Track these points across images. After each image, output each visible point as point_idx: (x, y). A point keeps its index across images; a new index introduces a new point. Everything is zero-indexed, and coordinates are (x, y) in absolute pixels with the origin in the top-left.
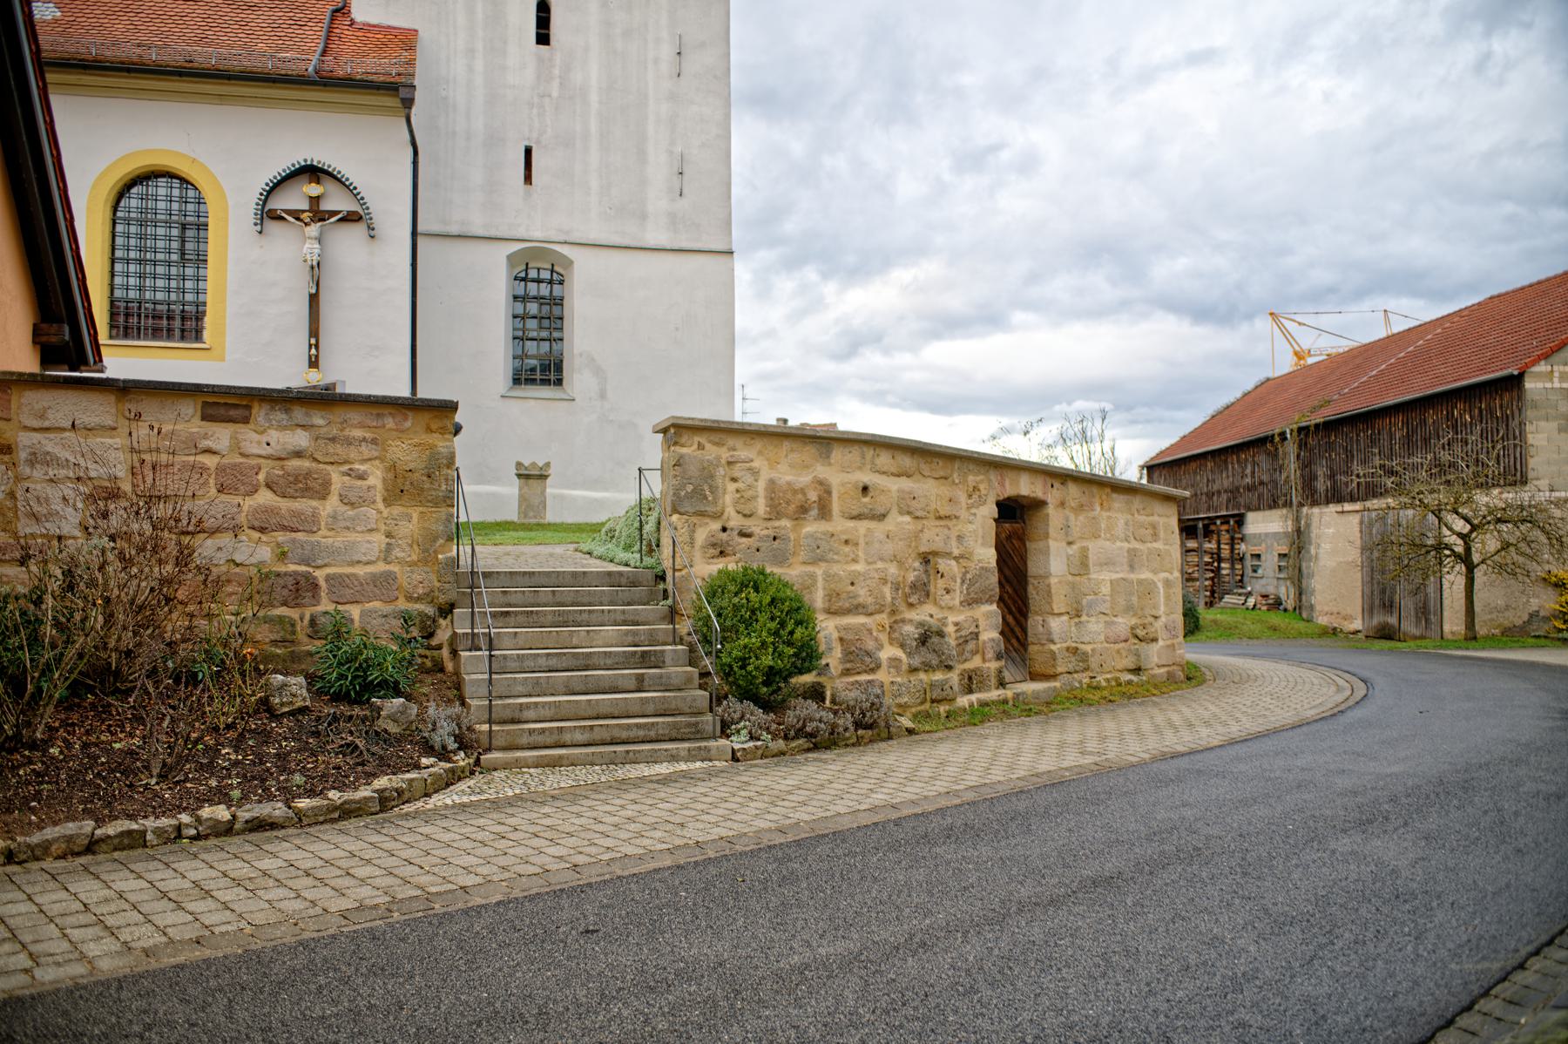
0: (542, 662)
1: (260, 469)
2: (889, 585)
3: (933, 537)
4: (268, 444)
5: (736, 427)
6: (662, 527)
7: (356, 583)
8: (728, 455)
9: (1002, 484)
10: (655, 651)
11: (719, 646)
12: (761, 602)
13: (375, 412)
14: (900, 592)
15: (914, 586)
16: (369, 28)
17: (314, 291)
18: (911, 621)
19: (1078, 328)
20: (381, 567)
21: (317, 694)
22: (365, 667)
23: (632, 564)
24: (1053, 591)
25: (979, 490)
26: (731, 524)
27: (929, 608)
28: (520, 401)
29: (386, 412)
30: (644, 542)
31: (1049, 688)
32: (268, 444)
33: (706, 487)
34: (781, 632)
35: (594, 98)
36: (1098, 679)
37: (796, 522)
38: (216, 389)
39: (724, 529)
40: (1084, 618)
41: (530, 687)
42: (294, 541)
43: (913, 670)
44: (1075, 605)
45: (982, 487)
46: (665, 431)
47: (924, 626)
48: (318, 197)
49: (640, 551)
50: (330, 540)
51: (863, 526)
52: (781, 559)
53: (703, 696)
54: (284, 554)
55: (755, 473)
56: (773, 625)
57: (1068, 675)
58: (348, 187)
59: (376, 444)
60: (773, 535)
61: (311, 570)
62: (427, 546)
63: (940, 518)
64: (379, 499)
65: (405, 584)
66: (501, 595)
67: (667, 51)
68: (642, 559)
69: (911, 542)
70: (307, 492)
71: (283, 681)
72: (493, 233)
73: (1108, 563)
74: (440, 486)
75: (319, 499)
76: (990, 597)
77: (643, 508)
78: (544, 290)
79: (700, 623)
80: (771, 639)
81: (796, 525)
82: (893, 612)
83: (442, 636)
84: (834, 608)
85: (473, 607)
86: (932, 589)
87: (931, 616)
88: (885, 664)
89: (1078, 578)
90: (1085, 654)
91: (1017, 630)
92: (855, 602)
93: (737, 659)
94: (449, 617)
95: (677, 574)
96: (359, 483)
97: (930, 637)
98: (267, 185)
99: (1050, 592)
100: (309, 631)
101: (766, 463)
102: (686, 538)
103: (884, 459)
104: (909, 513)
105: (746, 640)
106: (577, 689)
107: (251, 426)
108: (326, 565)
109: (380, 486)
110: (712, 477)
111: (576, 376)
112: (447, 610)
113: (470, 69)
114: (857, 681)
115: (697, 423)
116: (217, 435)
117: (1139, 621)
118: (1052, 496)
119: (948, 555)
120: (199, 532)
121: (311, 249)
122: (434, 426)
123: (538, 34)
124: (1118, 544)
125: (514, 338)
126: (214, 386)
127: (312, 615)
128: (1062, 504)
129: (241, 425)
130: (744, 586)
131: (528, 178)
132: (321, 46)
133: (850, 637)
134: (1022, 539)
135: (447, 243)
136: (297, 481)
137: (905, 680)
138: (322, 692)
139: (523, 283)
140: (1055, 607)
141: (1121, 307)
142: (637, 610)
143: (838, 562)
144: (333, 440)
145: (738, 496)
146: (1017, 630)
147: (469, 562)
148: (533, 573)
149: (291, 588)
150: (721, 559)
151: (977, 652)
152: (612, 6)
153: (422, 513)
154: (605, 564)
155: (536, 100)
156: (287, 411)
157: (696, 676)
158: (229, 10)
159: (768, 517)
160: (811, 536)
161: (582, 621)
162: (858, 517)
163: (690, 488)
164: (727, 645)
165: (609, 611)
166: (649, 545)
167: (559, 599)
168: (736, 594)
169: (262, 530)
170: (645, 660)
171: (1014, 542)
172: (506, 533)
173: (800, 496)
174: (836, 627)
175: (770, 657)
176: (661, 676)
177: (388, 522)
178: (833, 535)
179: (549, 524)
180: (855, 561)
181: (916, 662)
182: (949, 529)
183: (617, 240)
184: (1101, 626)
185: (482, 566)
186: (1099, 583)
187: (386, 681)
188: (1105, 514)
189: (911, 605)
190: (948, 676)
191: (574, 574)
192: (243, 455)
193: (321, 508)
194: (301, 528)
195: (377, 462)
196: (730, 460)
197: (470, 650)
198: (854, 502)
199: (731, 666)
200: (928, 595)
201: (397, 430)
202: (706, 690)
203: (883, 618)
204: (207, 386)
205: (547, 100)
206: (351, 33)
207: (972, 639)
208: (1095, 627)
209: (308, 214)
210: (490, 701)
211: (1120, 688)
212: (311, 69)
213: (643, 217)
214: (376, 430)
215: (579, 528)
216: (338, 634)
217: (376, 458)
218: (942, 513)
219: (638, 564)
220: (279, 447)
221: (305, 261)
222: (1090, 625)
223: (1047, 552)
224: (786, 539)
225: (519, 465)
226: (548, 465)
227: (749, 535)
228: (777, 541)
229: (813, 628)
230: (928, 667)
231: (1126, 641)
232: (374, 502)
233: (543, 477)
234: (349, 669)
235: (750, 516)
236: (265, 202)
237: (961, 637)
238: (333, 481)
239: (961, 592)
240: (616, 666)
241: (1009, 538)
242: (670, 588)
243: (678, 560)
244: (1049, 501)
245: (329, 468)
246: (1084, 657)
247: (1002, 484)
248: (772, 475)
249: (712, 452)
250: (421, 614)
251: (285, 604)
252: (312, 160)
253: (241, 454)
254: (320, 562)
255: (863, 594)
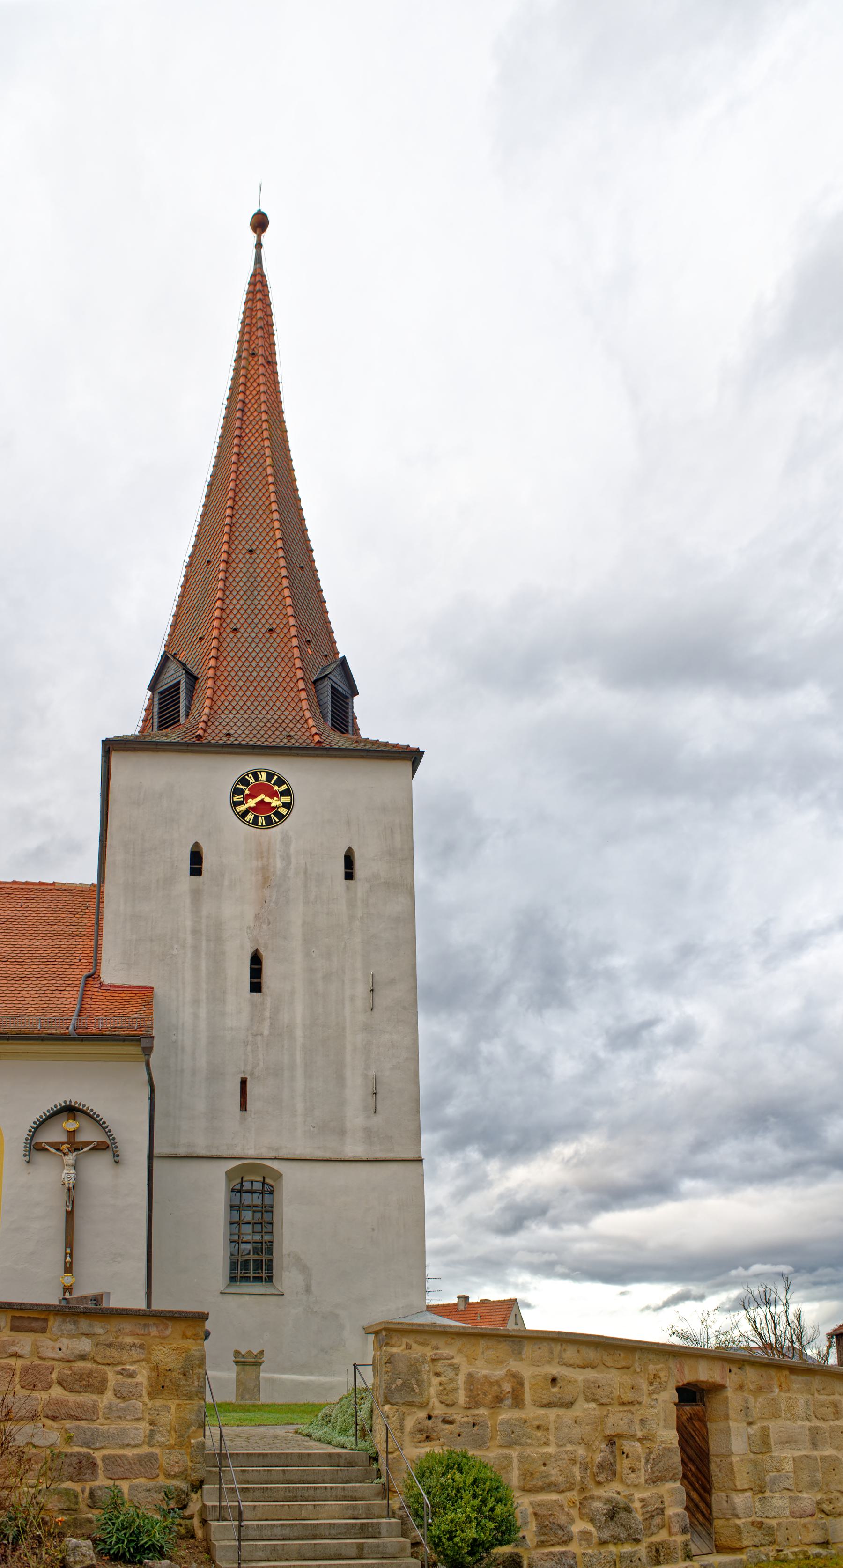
0: (277, 1532)
1: (53, 1369)
2: (578, 1465)
3: (617, 1420)
4: (60, 1349)
5: (439, 1329)
6: (374, 1414)
7: (126, 1462)
8: (432, 1353)
9: (681, 1371)
10: (372, 1523)
11: (430, 1521)
12: (465, 1482)
13: (142, 1322)
14: (588, 1471)
15: (601, 1466)
16: (114, 988)
17: (69, 1209)
18: (600, 1497)
19: (750, 1192)
20: (145, 1450)
21: (100, 1554)
22: (137, 1534)
23: (349, 1447)
24: (736, 1469)
25: (659, 1377)
26: (436, 1413)
27: (616, 1486)
28: (235, 1297)
29: (151, 1322)
30: (358, 1427)
31: (736, 1560)
32: (60, 1349)
33: (413, 1381)
34: (483, 1508)
35: (299, 1033)
36: (784, 1552)
37: (492, 1411)
38: (22, 1307)
39: (429, 1417)
40: (768, 1494)
41: (269, 1552)
42: (78, 1428)
43: (603, 1543)
44: (758, 1482)
45: (662, 1374)
46: (377, 1333)
47: (612, 1502)
48: (74, 1131)
49: (356, 1435)
50: (106, 1427)
51: (552, 1414)
52: (481, 1443)
53: (415, 1563)
54: (70, 1438)
55: (456, 1368)
56: (476, 1502)
57: (754, 1548)
58: (98, 1122)
59: (143, 1349)
60: (472, 1422)
61: (91, 1452)
62: (182, 1432)
63: (623, 1404)
64: (145, 1393)
65: (164, 1464)
66: (240, 1473)
67: (361, 990)
68: (357, 1442)
69: (597, 1426)
70: (89, 1388)
71: (76, 1543)
72: (214, 1153)
73: (789, 1441)
74: (193, 1382)
75: (99, 1393)
76: (674, 1474)
77: (358, 1395)
78: (257, 1200)
79: (412, 1500)
80: (474, 1515)
81: (493, 1413)
82: (583, 1490)
83: (194, 1507)
84: (528, 1486)
85: (220, 1483)
86: (618, 1468)
87: (618, 1493)
88: (576, 1537)
89: (760, 1456)
90: (770, 1528)
91: (702, 1505)
92: (547, 1481)
93: (445, 1532)
94: (199, 1492)
95: (390, 1456)
96: (129, 1380)
97: (618, 1513)
98: (35, 1123)
99: (733, 1470)
100: (89, 1501)
101: (465, 1359)
102: (396, 1425)
103: (571, 1354)
104: (594, 1400)
105: (453, 1515)
106: (308, 1556)
107: (48, 1335)
108: (102, 1448)
109: (145, 1383)
110: (418, 1372)
111: (285, 1274)
112: (197, 1486)
113: (196, 1016)
114: (551, 1553)
115: (405, 1327)
116: (22, 1342)
117: (824, 1497)
118: (731, 1380)
119: (633, 1437)
120: (7, 1420)
121: (68, 1173)
122: (189, 1333)
123: (251, 983)
124: (800, 1423)
125: (231, 1242)
126: (21, 1304)
127: (91, 1489)
128: (741, 1387)
129: (40, 1334)
130: (449, 1468)
131: (243, 1106)
132: (78, 1007)
133: (543, 1512)
134: (703, 1420)
135: (177, 1164)
136: (81, 1378)
137: (596, 1552)
138: (103, 1553)
139: (238, 1194)
140: (738, 1483)
141: (795, 1169)
142: (355, 1487)
143: (532, 1445)
144: (110, 1345)
145: (441, 1388)
146: (702, 1505)
147: (217, 1444)
148: (266, 1454)
149: (76, 1466)
150: (427, 1443)
151: (663, 1526)
152: (314, 955)
153: (178, 1405)
154: (325, 1446)
155: (250, 1038)
156: (75, 1323)
157: (409, 1545)
158: (6, 982)
159: (468, 1406)
160: (506, 1422)
161: (309, 1496)
162: (548, 1405)
163: (399, 1382)
164: (436, 1519)
165: (331, 1488)
166: (363, 1429)
167: (288, 1477)
168: (443, 1475)
169: (54, 1419)
170: (364, 1531)
171: (695, 1423)
172: (228, 1414)
173: (496, 1387)
174: (531, 1503)
175: (474, 1531)
176: (378, 1546)
177: (151, 1412)
178: (526, 1421)
179: (262, 1405)
180: (546, 1444)
181: (606, 1535)
182: (632, 1413)
183: (319, 1154)
184: (785, 1501)
185: (230, 1447)
186: (781, 1460)
187: (153, 1545)
188: (783, 1395)
189: (599, 1483)
190: (636, 1548)
191: (300, 1456)
192: (40, 1358)
193: (100, 1401)
194: (84, 1417)
195: (144, 1363)
196: (434, 1357)
197: (218, 1520)
198: (544, 1392)
199: (440, 1538)
200: (614, 1474)
201: (159, 1337)
202: (416, 1558)
203: (574, 1495)
204: (17, 1304)
205: (259, 1038)
206: (100, 994)
207: (658, 1514)
208: (779, 1502)
209: (66, 1145)
210: (239, 1564)
211: (808, 1561)
212: (71, 1028)
213: (342, 1133)
214: (143, 1337)
215: (289, 1408)
216: (116, 1505)
217: (143, 1360)
218: (625, 1399)
219: (354, 1447)
220: (68, 1352)
221: (64, 1184)
222: (774, 1501)
223: (727, 1432)
224: (484, 1425)
225: (237, 1353)
226: (262, 1353)
227: (451, 1422)
228: (477, 1427)
229: (512, 1505)
230: (617, 1540)
231: (812, 1515)
232: (141, 1396)
233: (257, 1364)
234: (125, 1534)
235: (452, 1405)
236: (32, 1137)
237: (647, 1512)
238: (109, 1378)
239: (646, 1471)
240: (339, 1536)
241: (690, 1419)
242: (383, 1468)
243: (390, 1444)
244: (727, 1385)
245: (106, 1368)
246: (770, 1531)
247: (681, 1371)
248: (471, 1370)
249: (418, 1351)
250: (177, 1489)
251: (71, 1479)
252: (71, 1101)
253: (39, 1357)
254: (98, 1445)
255: (554, 1473)
